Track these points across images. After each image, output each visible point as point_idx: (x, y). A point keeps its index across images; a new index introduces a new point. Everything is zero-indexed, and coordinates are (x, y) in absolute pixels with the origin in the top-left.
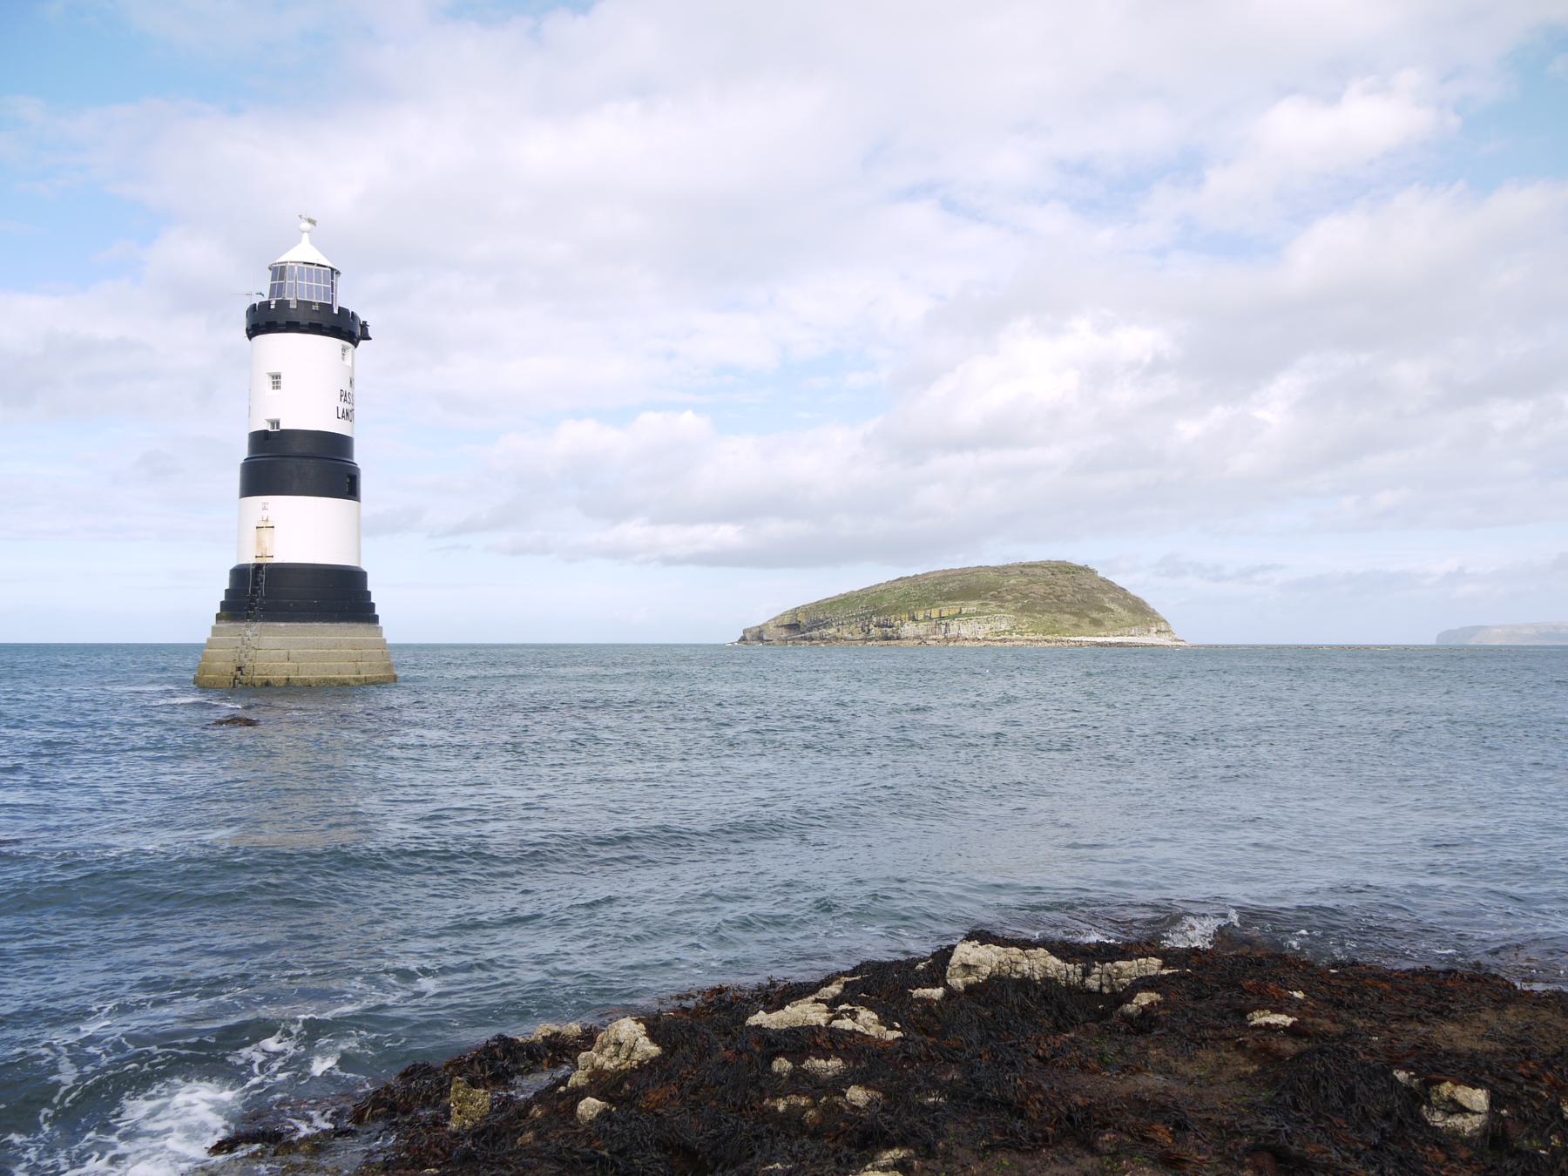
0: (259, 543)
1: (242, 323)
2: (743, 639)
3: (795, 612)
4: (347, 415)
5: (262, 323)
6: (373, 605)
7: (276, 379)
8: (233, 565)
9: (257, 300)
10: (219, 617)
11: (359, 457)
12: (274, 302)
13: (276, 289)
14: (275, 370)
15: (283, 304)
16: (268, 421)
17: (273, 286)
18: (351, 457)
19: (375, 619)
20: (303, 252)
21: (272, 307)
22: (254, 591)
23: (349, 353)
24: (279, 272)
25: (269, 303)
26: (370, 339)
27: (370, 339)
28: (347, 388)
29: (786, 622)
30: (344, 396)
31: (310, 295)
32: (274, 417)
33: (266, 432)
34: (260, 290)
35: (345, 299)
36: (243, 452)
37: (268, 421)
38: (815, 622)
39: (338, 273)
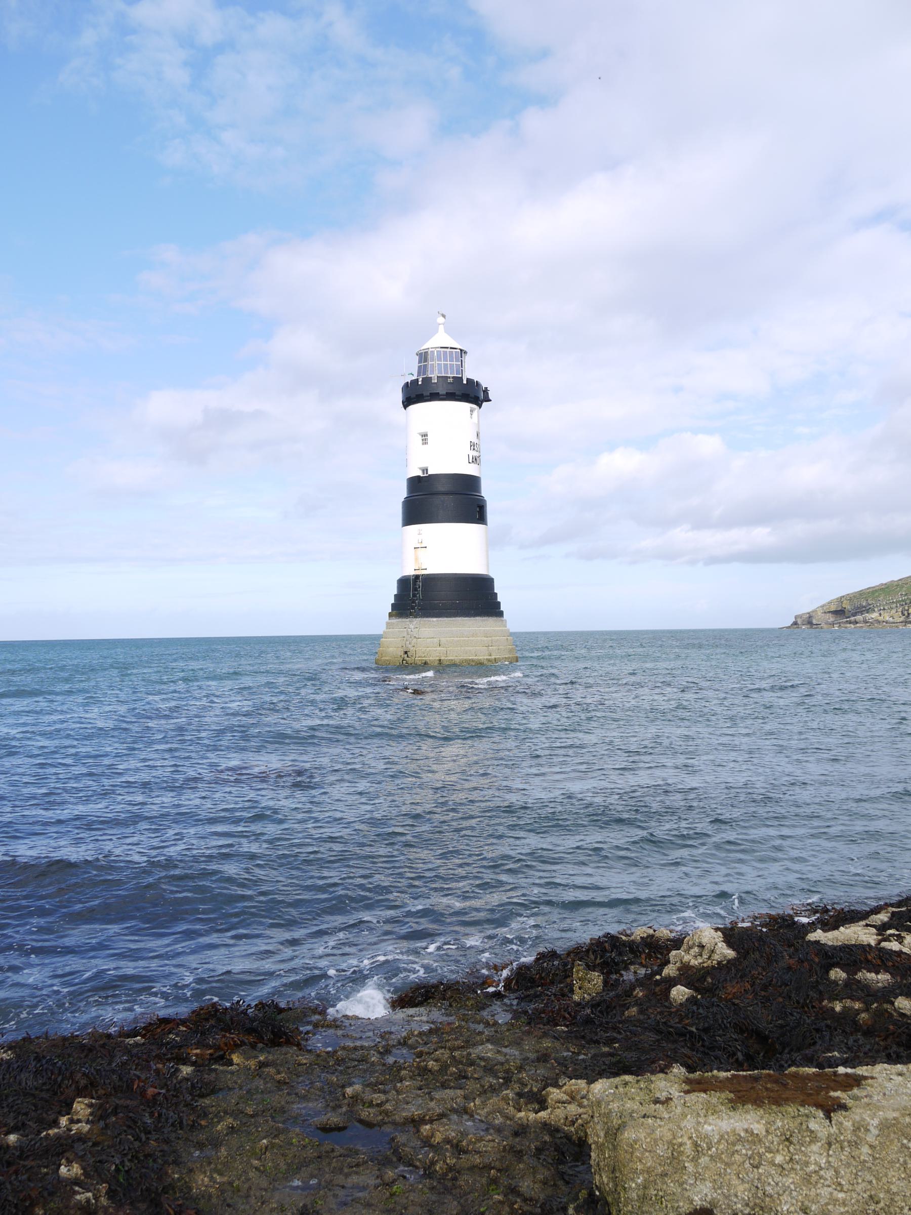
0: (416, 559)
1: (399, 397)
2: (795, 623)
3: (840, 600)
4: (475, 460)
5: (413, 396)
6: (499, 603)
7: (424, 436)
8: (399, 577)
9: (409, 379)
10: (390, 615)
11: (486, 491)
12: (420, 379)
13: (422, 370)
14: (423, 431)
15: (427, 380)
16: (420, 469)
17: (419, 367)
18: (480, 492)
19: (500, 614)
20: (441, 339)
21: (420, 383)
22: (414, 595)
23: (475, 413)
24: (423, 357)
25: (417, 380)
26: (490, 401)
27: (490, 401)
28: (475, 440)
29: (833, 608)
30: (473, 446)
31: (446, 372)
32: (424, 465)
33: (419, 477)
34: (410, 372)
35: (470, 372)
36: (403, 492)
37: (420, 469)
38: (858, 608)
39: (465, 353)
